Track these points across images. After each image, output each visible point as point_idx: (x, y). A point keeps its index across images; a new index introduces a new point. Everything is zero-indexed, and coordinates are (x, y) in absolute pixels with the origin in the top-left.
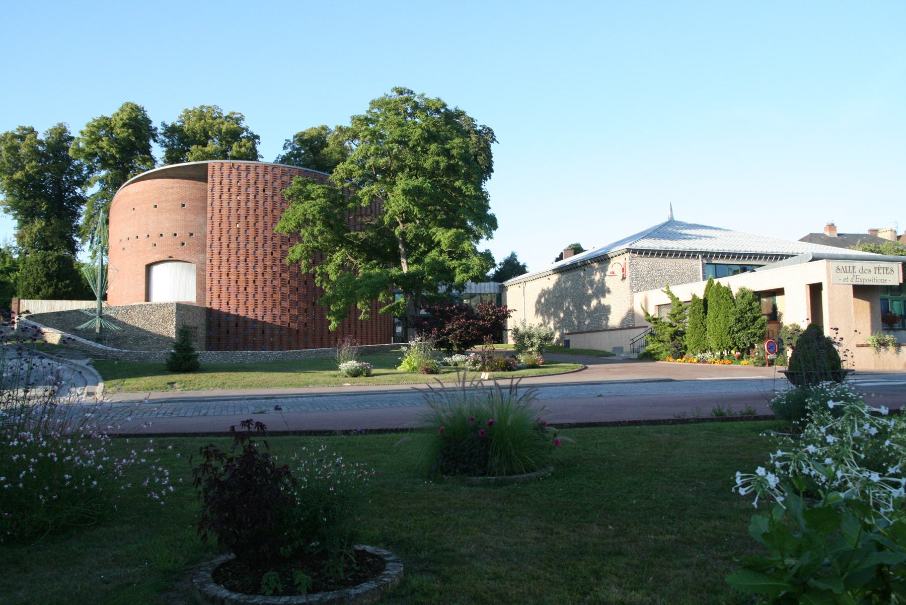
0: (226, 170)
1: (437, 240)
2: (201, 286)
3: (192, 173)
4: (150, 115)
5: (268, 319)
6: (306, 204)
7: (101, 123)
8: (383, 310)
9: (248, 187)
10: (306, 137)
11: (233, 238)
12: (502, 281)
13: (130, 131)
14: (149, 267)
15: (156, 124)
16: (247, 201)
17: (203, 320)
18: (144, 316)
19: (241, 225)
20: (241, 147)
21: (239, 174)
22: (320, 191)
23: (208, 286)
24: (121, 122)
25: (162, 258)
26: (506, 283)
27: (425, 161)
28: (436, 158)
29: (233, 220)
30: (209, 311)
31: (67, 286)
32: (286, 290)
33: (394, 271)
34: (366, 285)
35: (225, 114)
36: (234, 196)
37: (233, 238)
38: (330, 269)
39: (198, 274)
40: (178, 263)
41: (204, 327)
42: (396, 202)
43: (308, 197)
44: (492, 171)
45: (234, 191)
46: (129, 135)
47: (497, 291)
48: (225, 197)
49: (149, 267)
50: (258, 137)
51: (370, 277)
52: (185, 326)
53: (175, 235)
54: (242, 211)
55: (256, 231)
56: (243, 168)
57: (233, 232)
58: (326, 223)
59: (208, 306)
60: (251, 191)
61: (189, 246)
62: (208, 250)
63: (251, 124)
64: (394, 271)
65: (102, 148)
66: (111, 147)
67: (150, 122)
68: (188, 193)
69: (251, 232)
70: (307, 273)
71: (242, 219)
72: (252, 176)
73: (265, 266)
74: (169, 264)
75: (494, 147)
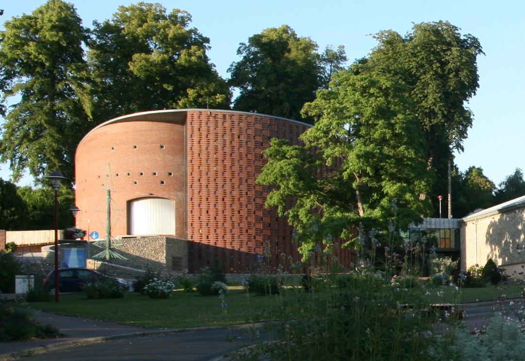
0: (204, 118)
1: (385, 192)
2: (182, 222)
3: (171, 118)
4: (80, 13)
5: (244, 249)
6: (282, 163)
7: (25, 23)
8: (346, 245)
9: (224, 133)
10: (264, 40)
11: (212, 179)
12: (460, 218)
13: (61, 34)
14: (129, 203)
15: (87, 23)
16: (224, 146)
17: (186, 251)
18: (139, 248)
19: (220, 168)
20: (190, 55)
21: (216, 122)
22: (293, 152)
23: (189, 221)
24: (50, 25)
25: (143, 195)
26: (465, 219)
27: (375, 133)
28: (384, 130)
29: (212, 162)
30: (191, 244)
31: (13, 214)
32: (252, 219)
33: (351, 215)
34: (330, 227)
35: (168, 13)
36: (211, 142)
37: (212, 179)
38: (302, 213)
39: (177, 210)
40: (157, 200)
41: (187, 257)
42: (353, 163)
43: (284, 157)
44: (478, 86)
45: (212, 137)
46: (60, 40)
47: (456, 227)
48: (204, 141)
49: (129, 203)
50: (207, 40)
51: (333, 220)
52: (174, 258)
53: (155, 174)
54: (220, 156)
55: (233, 173)
56: (220, 116)
57: (212, 174)
58: (300, 177)
59: (189, 239)
60: (228, 138)
61: (173, 184)
62: (189, 190)
63: (199, 24)
64: (351, 215)
65: (30, 54)
66: (40, 53)
67: (80, 20)
68: (166, 136)
69: (228, 175)
70: (283, 216)
71: (220, 162)
72: (227, 124)
73: (241, 205)
74: (149, 200)
75: (480, 60)
